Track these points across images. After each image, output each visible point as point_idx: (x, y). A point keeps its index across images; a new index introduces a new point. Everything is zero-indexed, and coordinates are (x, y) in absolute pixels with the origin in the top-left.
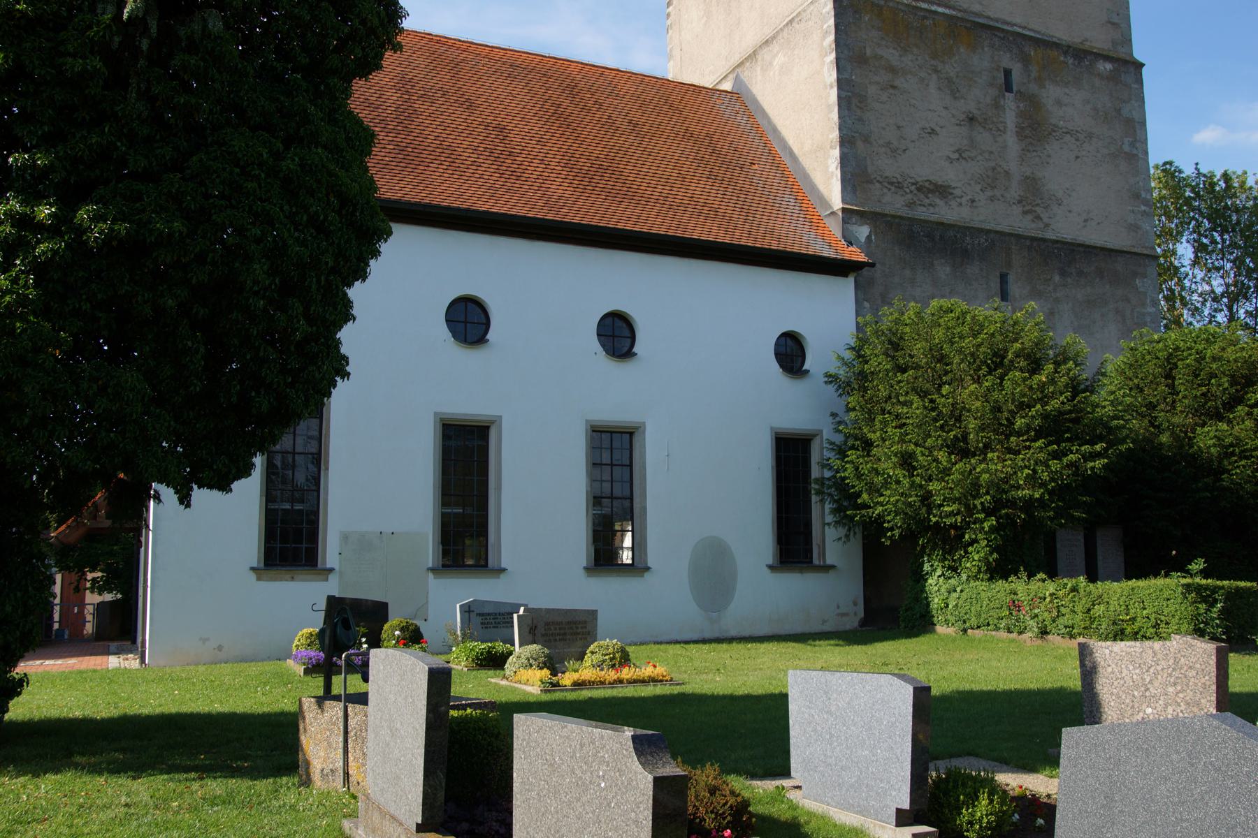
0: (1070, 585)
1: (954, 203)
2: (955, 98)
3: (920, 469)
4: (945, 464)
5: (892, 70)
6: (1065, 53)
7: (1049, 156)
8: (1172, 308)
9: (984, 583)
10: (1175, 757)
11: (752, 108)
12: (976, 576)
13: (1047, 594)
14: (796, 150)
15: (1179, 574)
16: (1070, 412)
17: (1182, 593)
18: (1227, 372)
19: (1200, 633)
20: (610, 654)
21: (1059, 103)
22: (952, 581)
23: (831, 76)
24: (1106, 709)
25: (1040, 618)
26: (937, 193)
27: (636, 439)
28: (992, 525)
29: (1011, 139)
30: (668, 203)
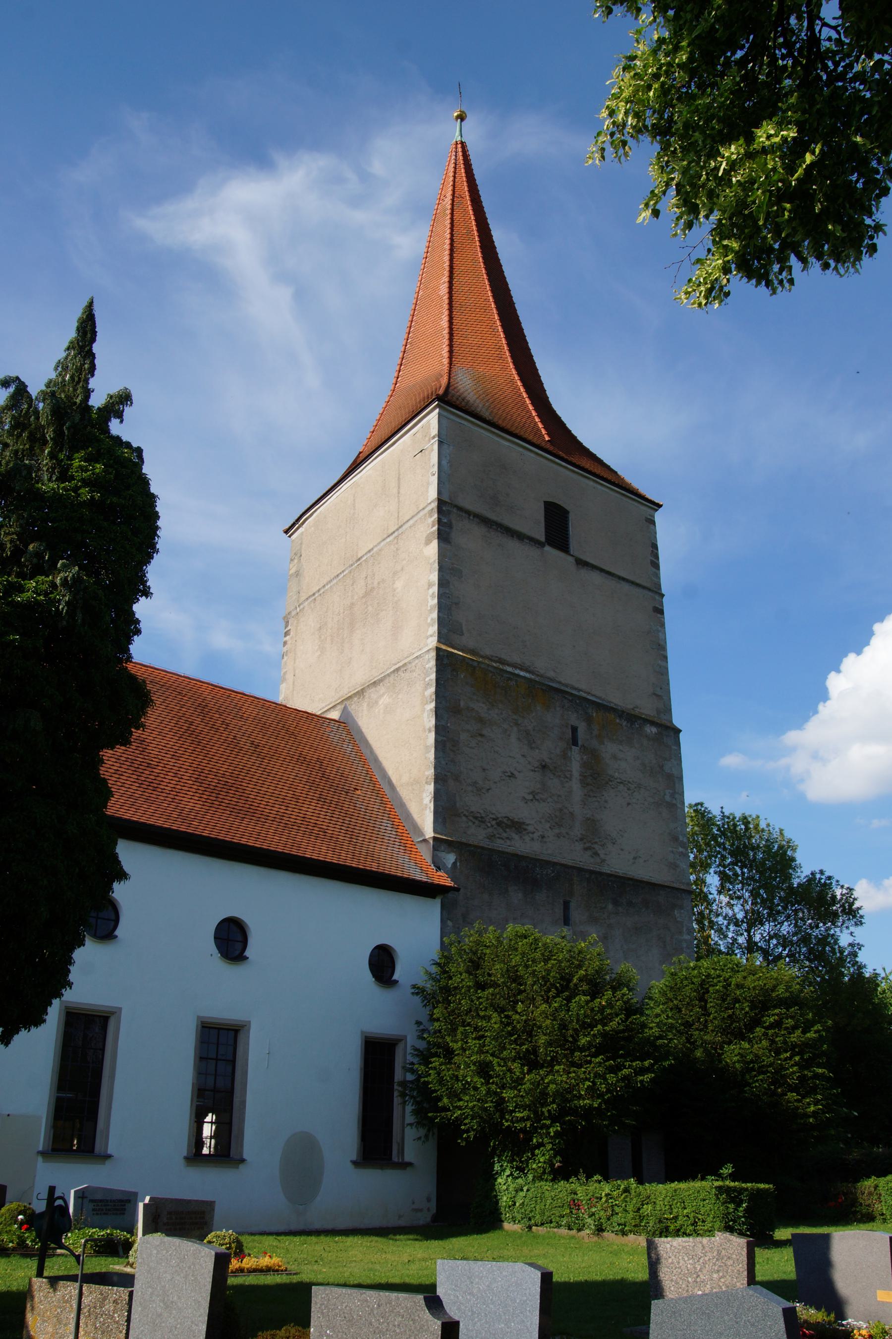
0: (622, 1187)
1: (527, 838)
2: (532, 748)
3: (496, 1077)
4: (518, 1074)
5: (481, 720)
6: (621, 717)
7: (606, 801)
8: (702, 929)
9: (548, 1183)
10: (726, 1318)
11: (357, 737)
12: (541, 1176)
13: (603, 1195)
14: (394, 780)
15: (713, 1177)
16: (623, 1031)
17: (715, 1195)
18: (748, 998)
19: (729, 1229)
20: (226, 1244)
21: (615, 757)
22: (520, 1181)
23: (430, 722)
24: (668, 1293)
25: (597, 1216)
26: (514, 829)
27: (241, 1036)
28: (557, 1130)
29: (575, 785)
30: (283, 821)
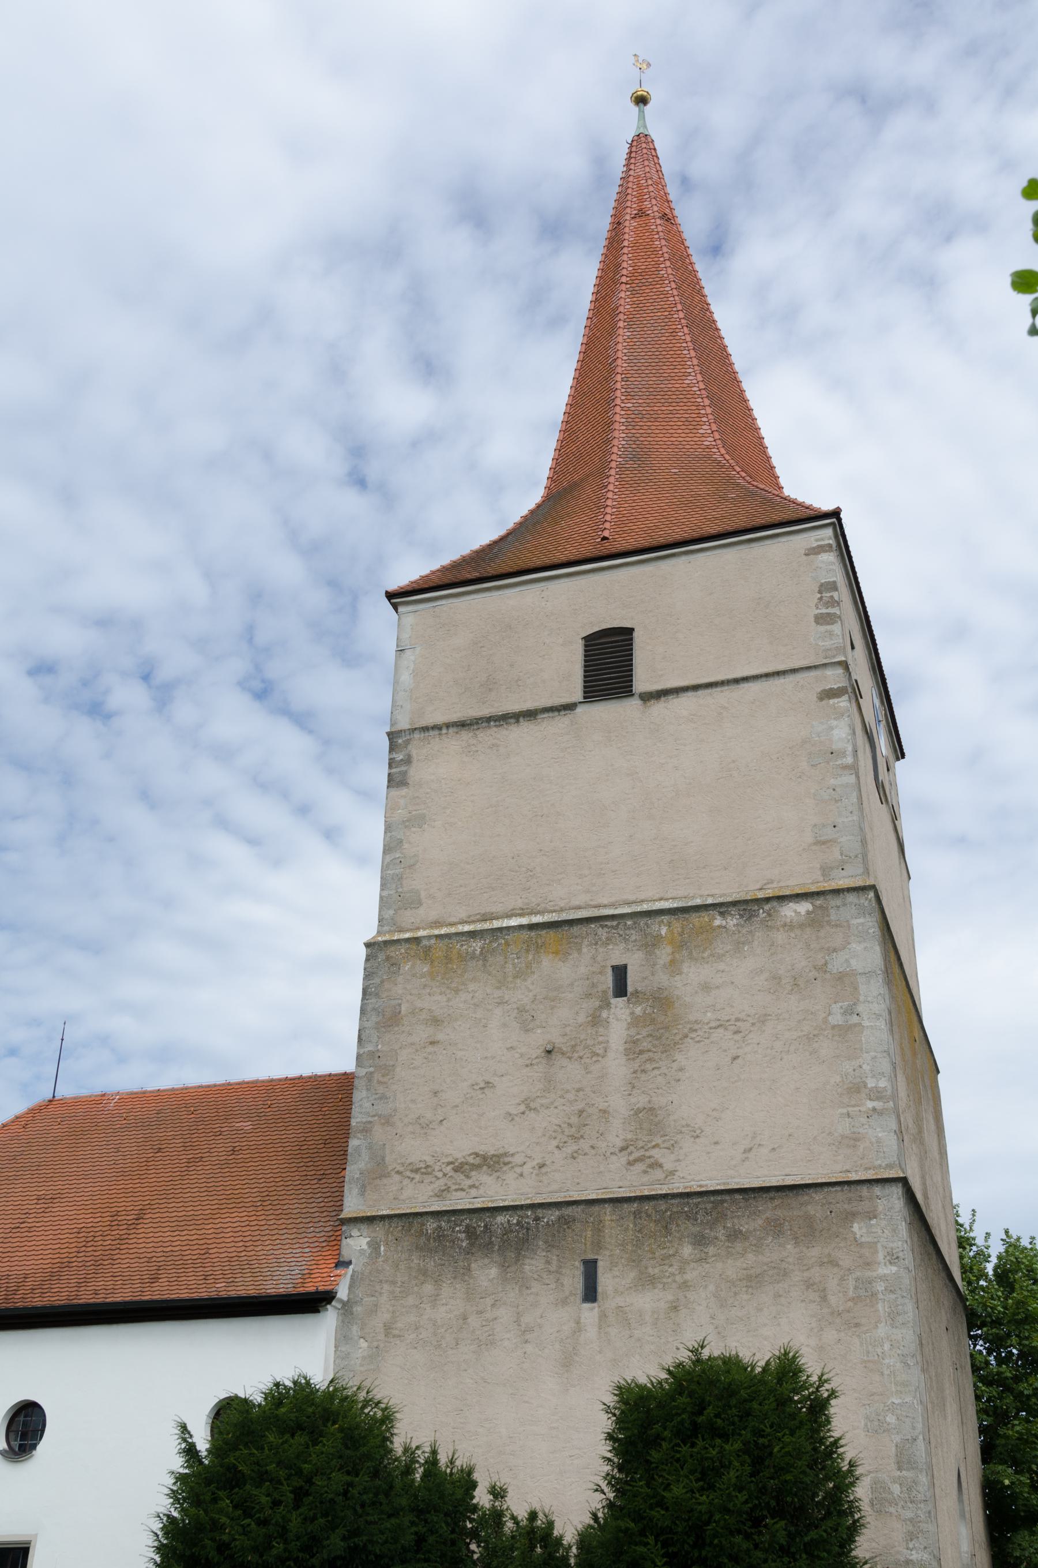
1: (510, 1176)
